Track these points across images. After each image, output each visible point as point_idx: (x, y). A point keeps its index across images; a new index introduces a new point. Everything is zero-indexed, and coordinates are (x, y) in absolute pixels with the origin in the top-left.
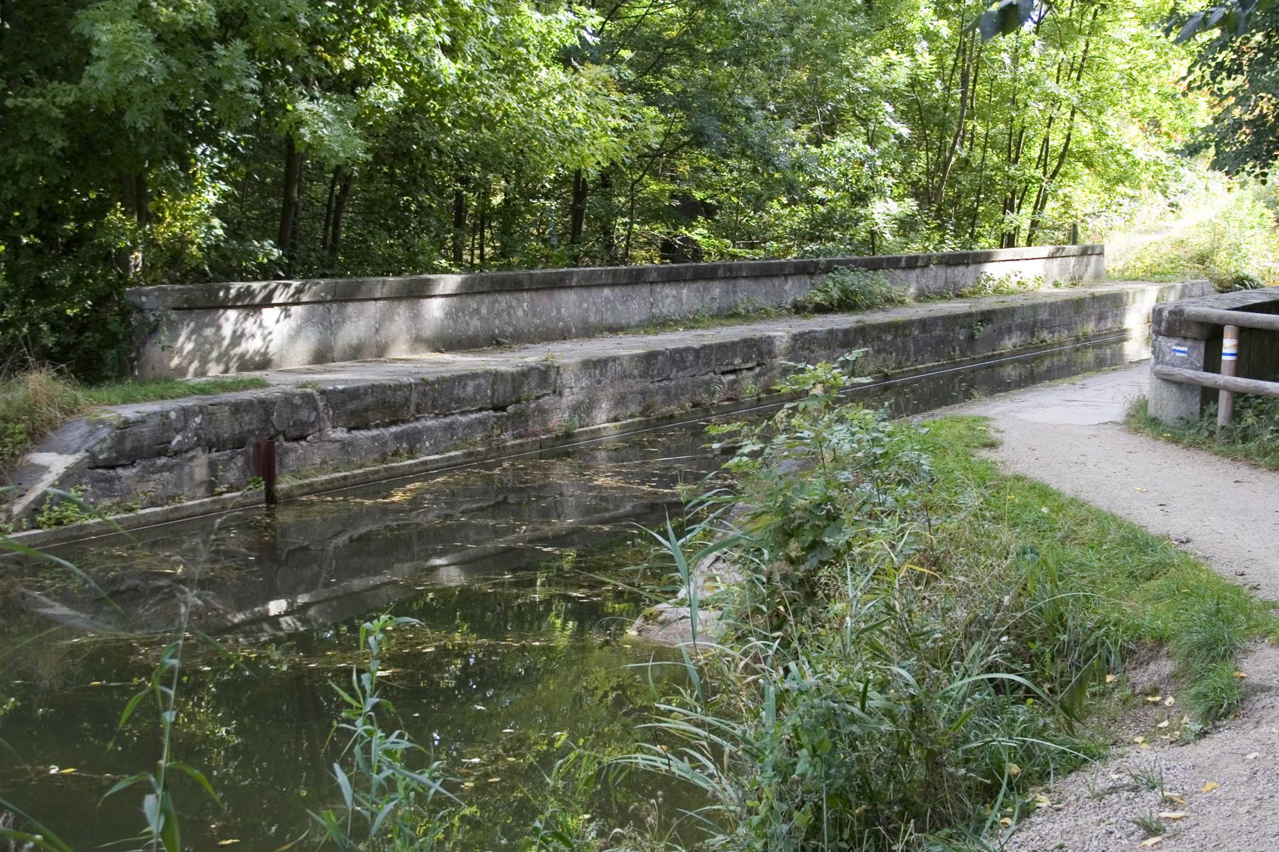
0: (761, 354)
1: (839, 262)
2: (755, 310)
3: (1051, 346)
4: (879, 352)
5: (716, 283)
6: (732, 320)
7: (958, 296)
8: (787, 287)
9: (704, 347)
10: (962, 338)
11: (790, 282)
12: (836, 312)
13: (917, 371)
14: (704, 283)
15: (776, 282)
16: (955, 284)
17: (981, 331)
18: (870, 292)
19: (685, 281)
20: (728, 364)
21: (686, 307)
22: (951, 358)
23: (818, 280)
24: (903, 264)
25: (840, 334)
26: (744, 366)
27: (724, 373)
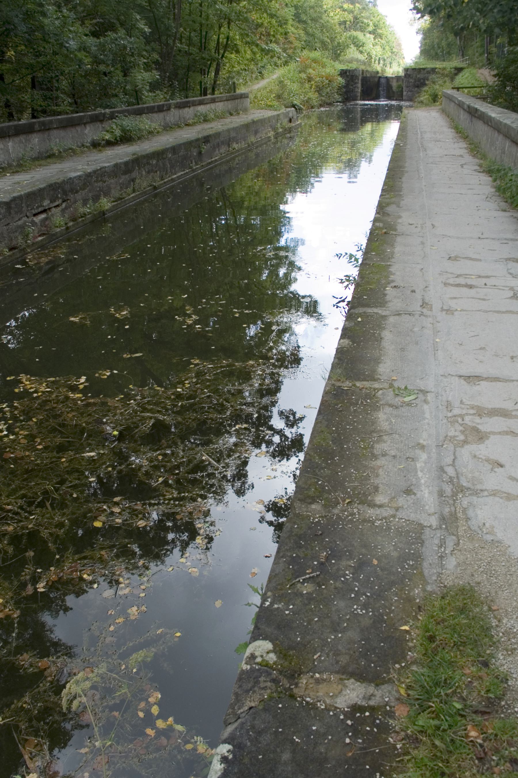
0: (65, 193)
1: (118, 112)
2: (65, 151)
3: (238, 151)
4: (148, 172)
5: (34, 135)
6: (49, 160)
7: (186, 125)
8: (86, 131)
9: (14, 199)
10: (195, 154)
11: (88, 128)
12: (119, 145)
13: (173, 180)
14: (24, 136)
15: (79, 129)
16: (184, 118)
17: (205, 148)
18: (139, 129)
19: (9, 136)
20: (38, 207)
21: (13, 156)
22: (191, 168)
23: (106, 125)
24: (156, 109)
25: (123, 166)
26: (52, 205)
27: (35, 215)
